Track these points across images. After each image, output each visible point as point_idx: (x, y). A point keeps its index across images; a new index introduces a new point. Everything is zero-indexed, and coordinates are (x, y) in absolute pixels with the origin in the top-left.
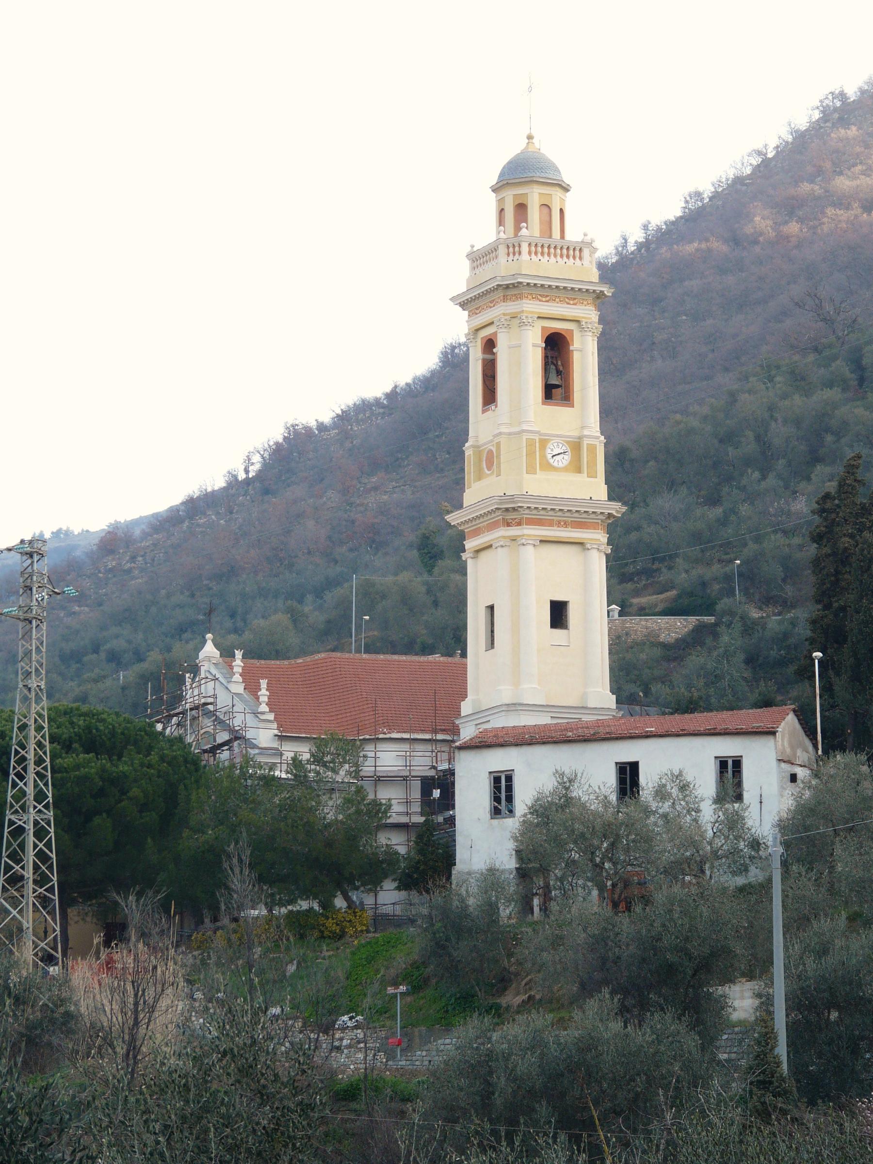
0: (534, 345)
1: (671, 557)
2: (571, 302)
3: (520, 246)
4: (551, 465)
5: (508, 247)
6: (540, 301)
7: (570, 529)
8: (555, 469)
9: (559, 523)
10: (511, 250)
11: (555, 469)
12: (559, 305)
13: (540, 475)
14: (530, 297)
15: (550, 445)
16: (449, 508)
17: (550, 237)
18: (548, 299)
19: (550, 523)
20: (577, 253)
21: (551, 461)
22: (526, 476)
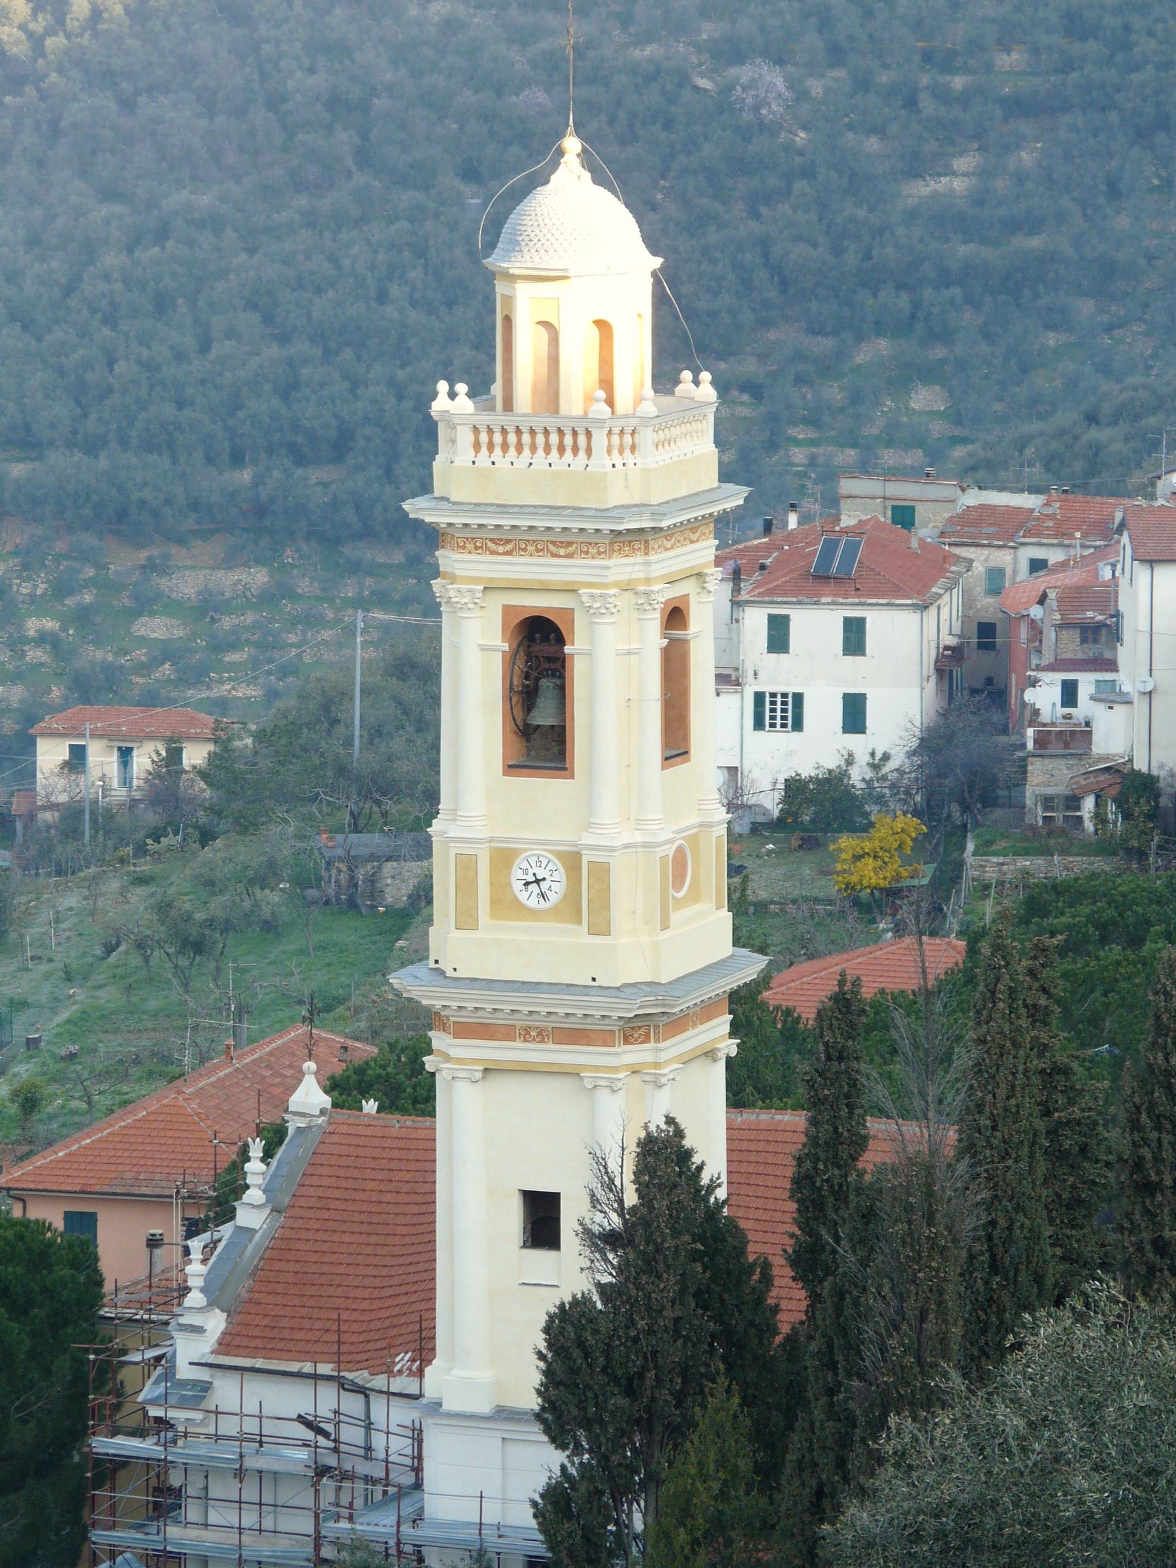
0: (484, 648)
1: (312, 1021)
2: (562, 552)
3: (589, 434)
4: (522, 905)
5: (476, 430)
6: (493, 553)
7: (550, 1046)
8: (532, 914)
9: (527, 1033)
10: (484, 437)
11: (532, 914)
12: (534, 560)
13: (489, 929)
14: (470, 546)
15: (520, 862)
16: (888, 1105)
17: (555, 411)
18: (509, 547)
19: (507, 1033)
20: (582, 440)
21: (522, 896)
22: (456, 935)
